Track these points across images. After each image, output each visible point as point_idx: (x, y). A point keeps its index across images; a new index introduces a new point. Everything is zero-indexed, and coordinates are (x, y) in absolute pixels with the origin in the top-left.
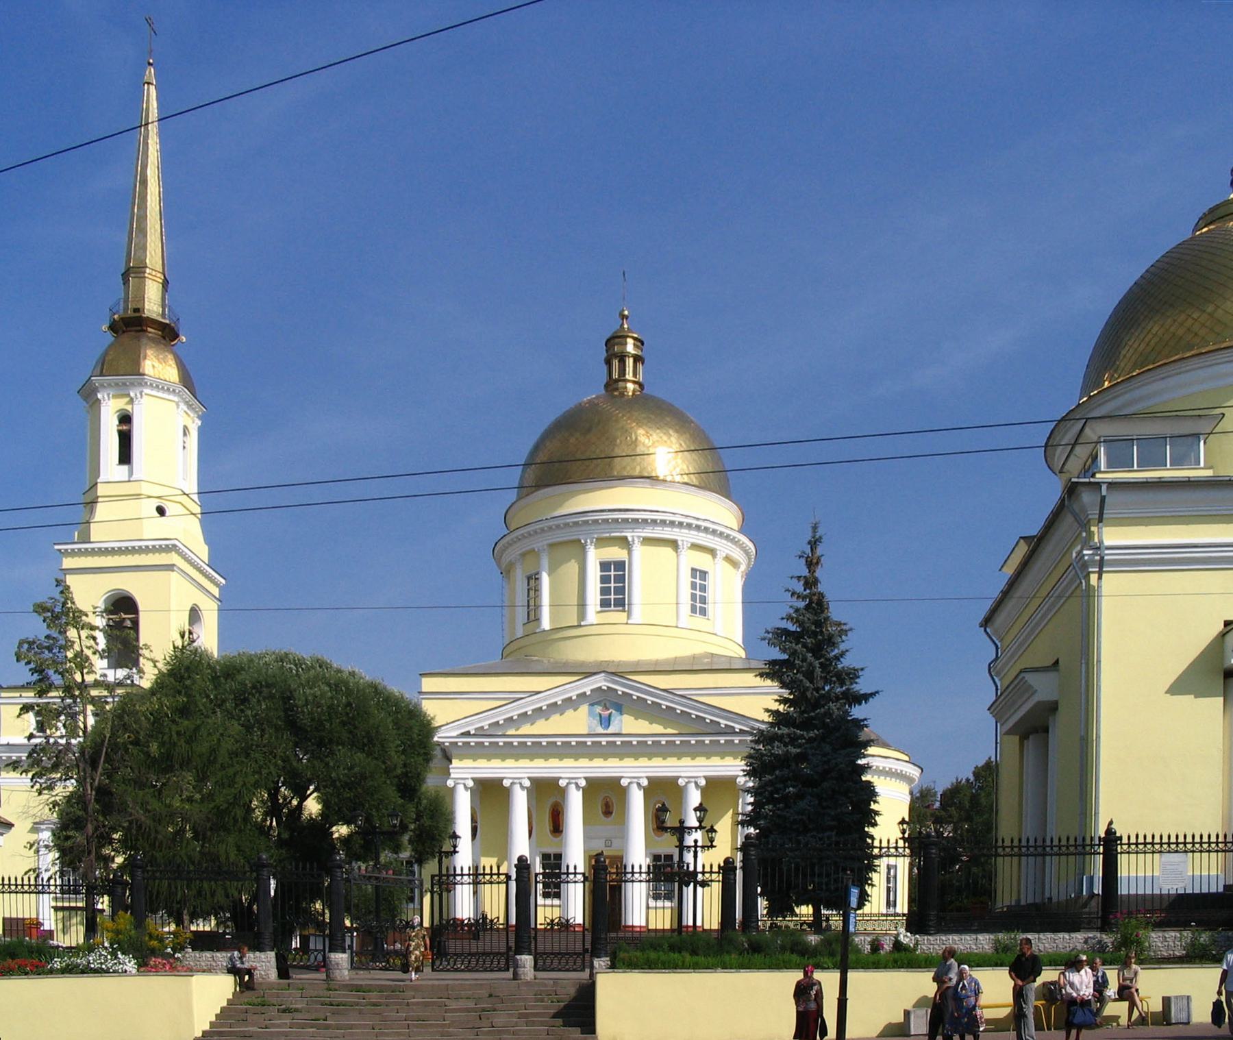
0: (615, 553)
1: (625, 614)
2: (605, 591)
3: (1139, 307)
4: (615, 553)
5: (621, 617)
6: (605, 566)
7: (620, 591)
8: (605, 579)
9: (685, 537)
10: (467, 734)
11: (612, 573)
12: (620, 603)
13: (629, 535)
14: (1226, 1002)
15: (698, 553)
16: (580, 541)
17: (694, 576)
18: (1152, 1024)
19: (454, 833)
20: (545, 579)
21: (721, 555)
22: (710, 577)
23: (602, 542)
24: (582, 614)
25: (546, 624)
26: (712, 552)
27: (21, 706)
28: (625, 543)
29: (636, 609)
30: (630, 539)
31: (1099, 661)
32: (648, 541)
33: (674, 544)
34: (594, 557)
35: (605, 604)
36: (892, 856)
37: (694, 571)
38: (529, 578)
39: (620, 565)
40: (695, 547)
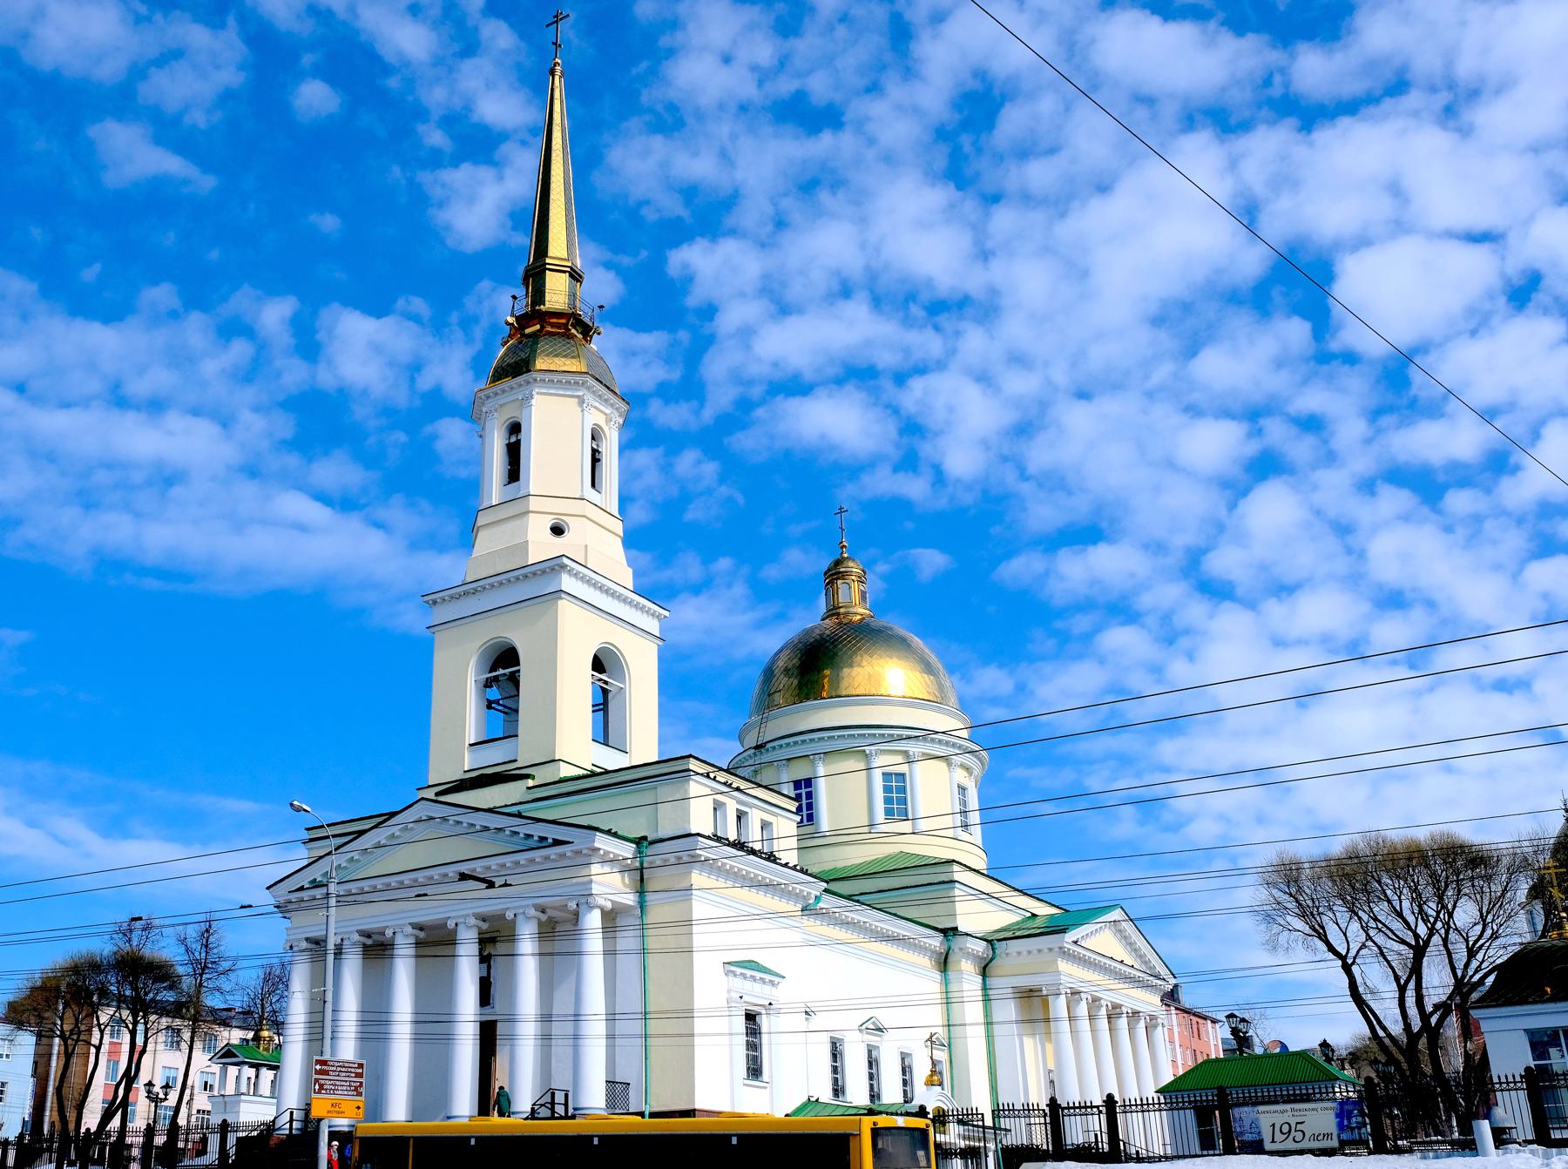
2: (888, 801)
8: (887, 789)
35: (889, 812)
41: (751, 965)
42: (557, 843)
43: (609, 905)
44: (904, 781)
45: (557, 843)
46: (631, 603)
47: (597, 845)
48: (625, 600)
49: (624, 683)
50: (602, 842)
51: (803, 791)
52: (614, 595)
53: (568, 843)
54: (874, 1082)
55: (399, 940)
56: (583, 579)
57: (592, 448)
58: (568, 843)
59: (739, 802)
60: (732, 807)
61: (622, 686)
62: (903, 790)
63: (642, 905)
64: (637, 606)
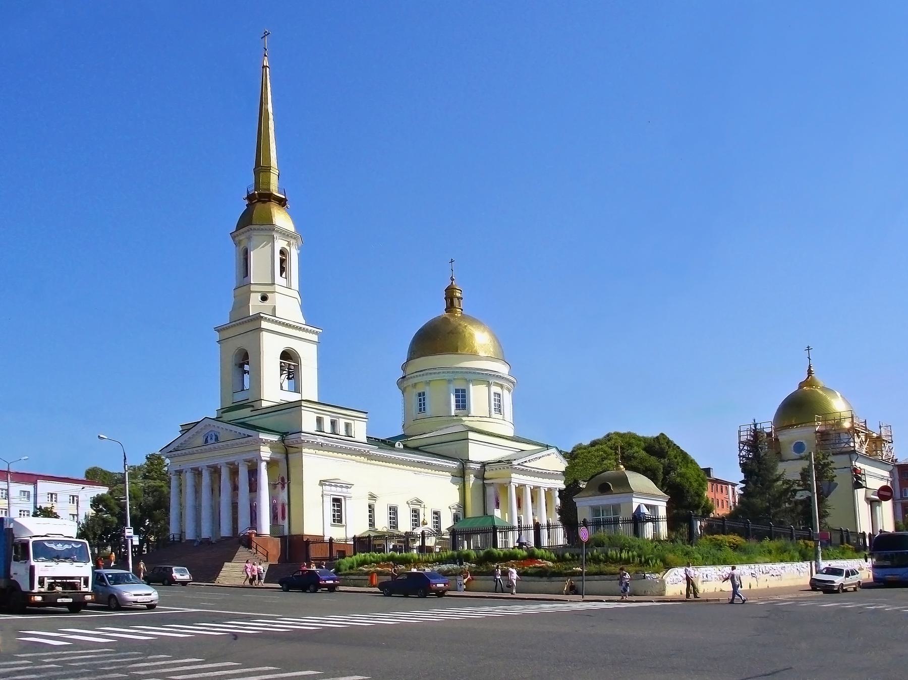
2: (457, 401)
6: (457, 391)
37: (495, 393)
42: (249, 436)
45: (249, 436)
50: (263, 436)
56: (273, 321)
62: (464, 396)
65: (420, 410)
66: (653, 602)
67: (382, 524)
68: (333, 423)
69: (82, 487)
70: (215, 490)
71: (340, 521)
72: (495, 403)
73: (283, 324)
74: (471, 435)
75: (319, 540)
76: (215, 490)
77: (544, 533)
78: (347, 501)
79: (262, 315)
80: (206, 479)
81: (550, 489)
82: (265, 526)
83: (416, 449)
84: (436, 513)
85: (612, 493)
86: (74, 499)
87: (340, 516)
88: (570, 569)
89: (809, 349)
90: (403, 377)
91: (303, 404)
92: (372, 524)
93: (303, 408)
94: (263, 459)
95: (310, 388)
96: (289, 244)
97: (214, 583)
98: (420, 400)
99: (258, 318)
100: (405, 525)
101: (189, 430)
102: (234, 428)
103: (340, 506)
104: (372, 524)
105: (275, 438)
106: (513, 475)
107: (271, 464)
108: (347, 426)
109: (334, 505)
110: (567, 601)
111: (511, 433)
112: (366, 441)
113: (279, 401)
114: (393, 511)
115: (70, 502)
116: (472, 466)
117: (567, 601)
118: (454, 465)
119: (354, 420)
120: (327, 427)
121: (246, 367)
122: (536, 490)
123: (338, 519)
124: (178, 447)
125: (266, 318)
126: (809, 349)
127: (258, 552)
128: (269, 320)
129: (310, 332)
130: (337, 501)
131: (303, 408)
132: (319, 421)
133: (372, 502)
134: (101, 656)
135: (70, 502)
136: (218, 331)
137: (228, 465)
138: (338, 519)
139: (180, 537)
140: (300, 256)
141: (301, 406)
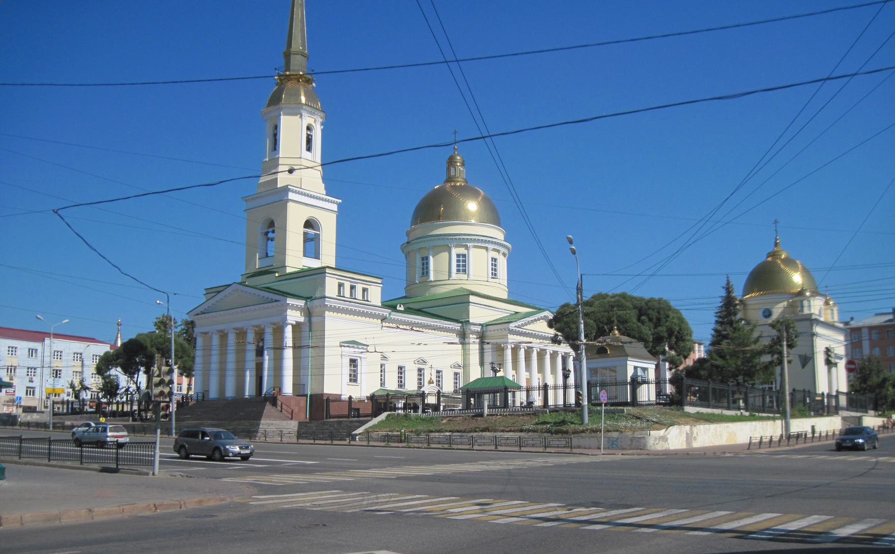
0: (462, 251)
1: (466, 275)
2: (458, 266)
3: (768, 399)
4: (462, 251)
5: (465, 277)
6: (458, 256)
7: (464, 266)
8: (458, 261)
9: (490, 246)
10: (516, 326)
11: (461, 259)
12: (464, 271)
13: (469, 244)
14: (534, 499)
15: (819, 380)
16: (448, 245)
17: (492, 261)
18: (604, 449)
19: (569, 370)
20: (431, 259)
21: (501, 252)
22: (498, 261)
23: (457, 246)
24: (450, 276)
25: (432, 278)
26: (498, 251)
27: (120, 387)
28: (467, 248)
29: (471, 273)
30: (469, 246)
31: (818, 388)
32: (475, 247)
33: (487, 249)
34: (455, 251)
35: (458, 271)
36: (111, 448)
37: (492, 258)
38: (423, 259)
39: (464, 256)
40: (494, 250)
41: (354, 342)
42: (276, 301)
43: (294, 323)
44: (466, 258)
45: (276, 301)
46: (326, 200)
47: (288, 302)
48: (322, 199)
49: (319, 231)
50: (290, 301)
51: (425, 262)
52: (317, 198)
53: (279, 301)
54: (383, 378)
55: (249, 331)
56: (299, 193)
57: (307, 133)
58: (279, 301)
59: (351, 282)
60: (347, 286)
61: (318, 233)
62: (464, 261)
63: (310, 321)
64: (328, 201)
65: (423, 273)
66: (615, 454)
67: (392, 385)
68: (352, 288)
69: (87, 345)
70: (241, 351)
71: (355, 381)
72: (496, 271)
73: (308, 195)
74: (472, 299)
75: (337, 399)
76: (241, 351)
77: (551, 393)
78: (343, 359)
79: (289, 187)
80: (232, 339)
81: (542, 350)
82: (288, 388)
83: (419, 312)
84: (438, 372)
85: (608, 356)
86: (79, 356)
87: (356, 376)
88: (852, 440)
89: (776, 222)
90: (408, 243)
91: (328, 270)
92: (383, 384)
93: (327, 275)
94: (289, 322)
95: (328, 256)
96: (315, 121)
97: (255, 439)
98: (423, 264)
99: (286, 189)
100: (411, 386)
101: (219, 292)
102: (262, 293)
103: (355, 366)
104: (383, 384)
105: (301, 303)
106: (509, 336)
107: (297, 327)
108: (364, 290)
109: (350, 365)
110: (589, 455)
111: (505, 296)
112: (380, 305)
113: (301, 267)
114: (401, 369)
115: (74, 360)
116: (473, 328)
117: (589, 455)
118: (457, 326)
119: (370, 285)
120: (347, 293)
121: (270, 235)
122: (542, 352)
123: (353, 378)
124: (205, 309)
125: (293, 190)
126: (776, 222)
127: (283, 410)
128: (296, 192)
129: (331, 202)
130: (353, 362)
131: (327, 275)
132: (340, 285)
133: (383, 362)
134: (335, 496)
135: (74, 360)
136: (246, 201)
137: (254, 328)
138: (353, 378)
139: (203, 395)
140: (323, 132)
141: (326, 273)
